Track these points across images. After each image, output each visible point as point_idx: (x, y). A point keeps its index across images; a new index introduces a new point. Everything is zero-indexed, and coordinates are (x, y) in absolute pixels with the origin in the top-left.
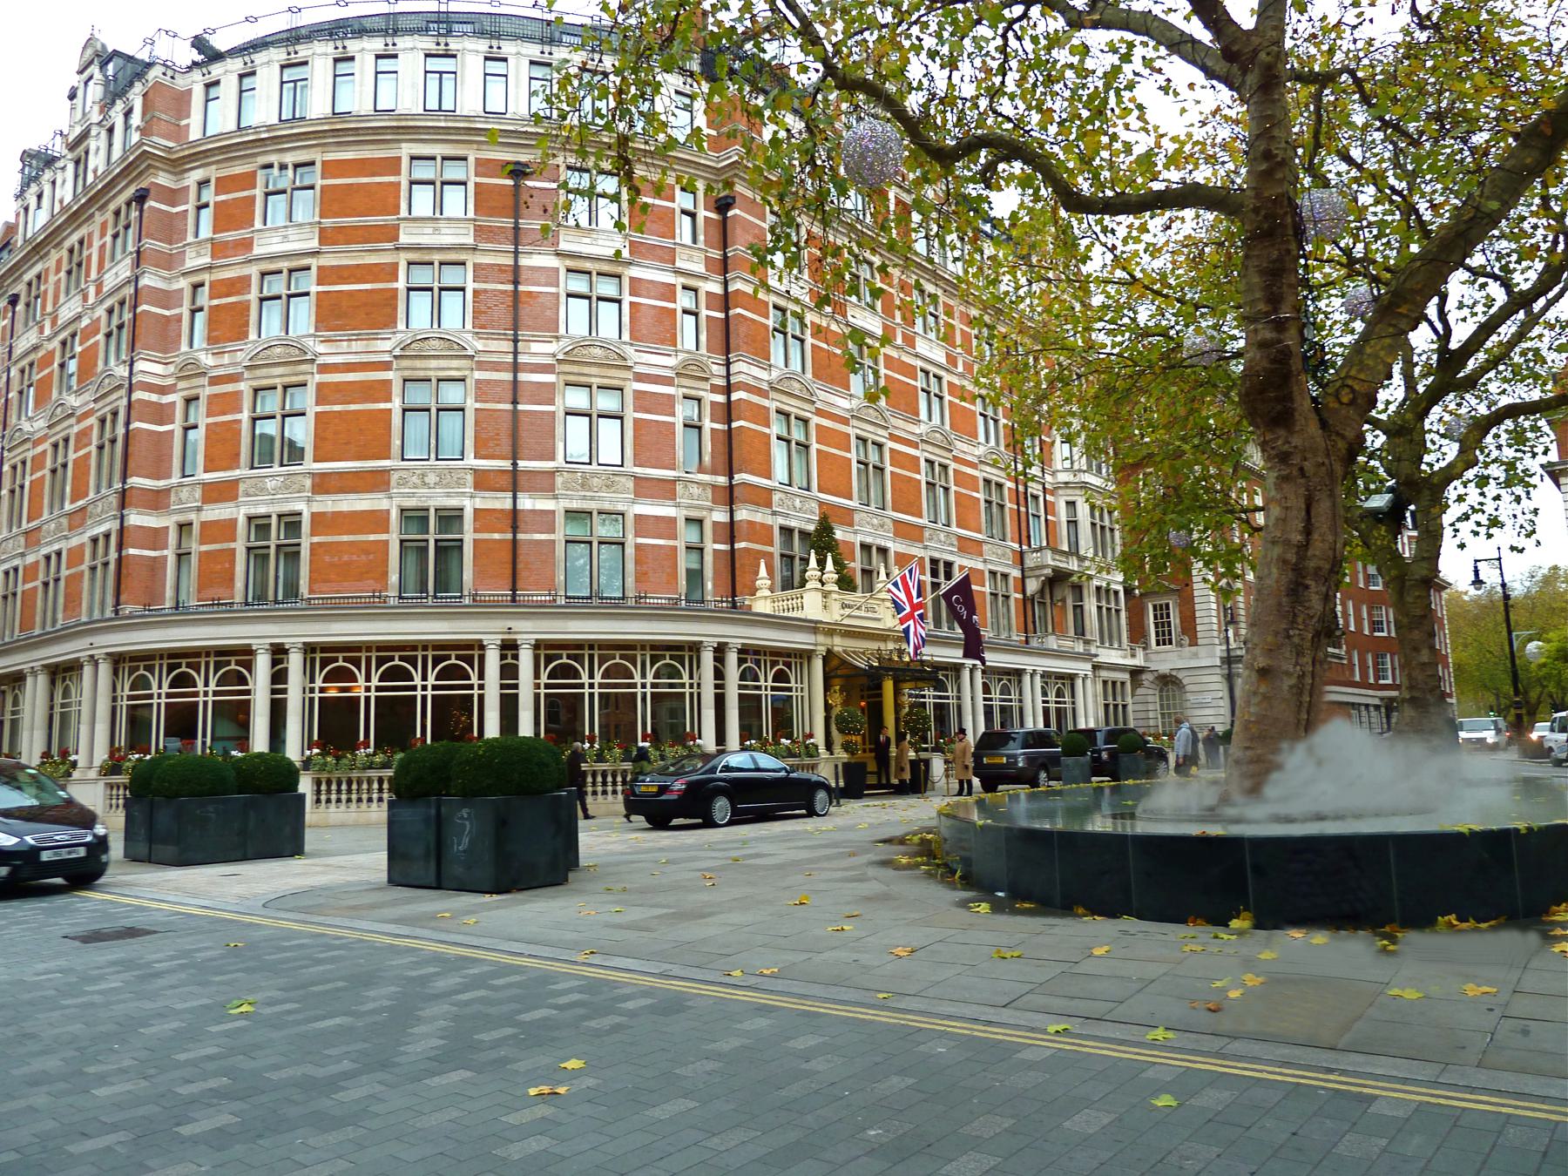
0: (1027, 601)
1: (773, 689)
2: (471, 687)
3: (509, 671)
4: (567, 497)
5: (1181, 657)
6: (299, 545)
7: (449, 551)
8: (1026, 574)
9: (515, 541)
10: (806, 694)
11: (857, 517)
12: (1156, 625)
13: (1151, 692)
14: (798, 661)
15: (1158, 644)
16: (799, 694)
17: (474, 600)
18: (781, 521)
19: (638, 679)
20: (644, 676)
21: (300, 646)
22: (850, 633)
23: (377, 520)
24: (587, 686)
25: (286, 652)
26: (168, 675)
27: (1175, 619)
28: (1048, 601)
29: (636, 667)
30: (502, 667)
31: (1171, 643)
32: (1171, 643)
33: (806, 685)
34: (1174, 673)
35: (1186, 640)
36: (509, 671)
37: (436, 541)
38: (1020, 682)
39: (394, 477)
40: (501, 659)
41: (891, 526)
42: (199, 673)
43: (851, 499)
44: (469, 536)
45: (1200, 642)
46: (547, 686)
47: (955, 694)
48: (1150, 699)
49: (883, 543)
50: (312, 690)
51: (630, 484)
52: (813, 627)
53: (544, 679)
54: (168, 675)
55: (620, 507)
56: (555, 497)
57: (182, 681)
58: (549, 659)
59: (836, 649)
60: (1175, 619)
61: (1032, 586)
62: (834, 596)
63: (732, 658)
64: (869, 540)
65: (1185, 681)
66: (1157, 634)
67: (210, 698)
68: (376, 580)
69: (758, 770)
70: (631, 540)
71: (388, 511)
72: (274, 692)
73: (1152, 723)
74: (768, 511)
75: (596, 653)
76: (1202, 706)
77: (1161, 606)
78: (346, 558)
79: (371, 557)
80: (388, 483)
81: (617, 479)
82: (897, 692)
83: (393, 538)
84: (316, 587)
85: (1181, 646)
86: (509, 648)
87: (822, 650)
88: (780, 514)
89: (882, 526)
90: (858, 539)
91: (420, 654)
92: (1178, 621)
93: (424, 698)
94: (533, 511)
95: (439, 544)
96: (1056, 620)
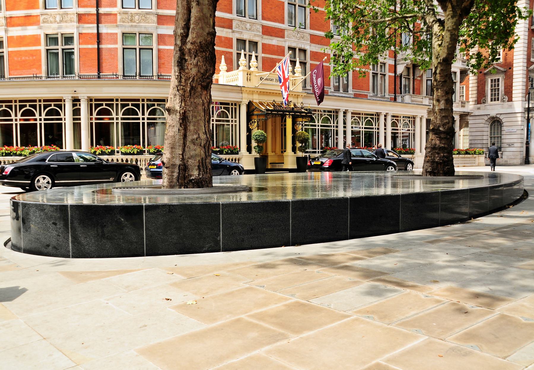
0: (397, 78)
1: (321, 126)
2: (139, 119)
3: (76, 112)
4: (122, 26)
5: (503, 108)
6: (3, 52)
7: (68, 55)
8: (397, 63)
9: (99, 49)
10: (238, 123)
11: (286, 33)
12: (492, 90)
13: (486, 126)
14: (234, 107)
15: (492, 100)
16: (234, 123)
17: (158, 78)
18: (238, 36)
19: (140, 116)
20: (143, 114)
21: (86, 98)
22: (263, 93)
23: (35, 40)
24: (141, 119)
25: (79, 100)
26: (44, 111)
27: (502, 87)
28: (411, 77)
29: (36, 110)
30: (74, 111)
31: (498, 100)
32: (498, 100)
33: (238, 119)
34: (498, 116)
35: (506, 98)
36: (76, 112)
37: (63, 49)
38: (378, 119)
39: (42, 18)
40: (73, 107)
41: (309, 37)
42: (36, 110)
43: (283, 22)
44: (76, 46)
45: (513, 99)
46: (45, 120)
47: (335, 124)
48: (486, 129)
49: (303, 47)
50: (91, 119)
51: (155, 19)
52: (240, 89)
53: (95, 115)
54: (44, 111)
55: (150, 31)
56: (117, 26)
57: (28, 113)
58: (97, 106)
59: (255, 101)
60: (502, 87)
61: (400, 69)
62: (254, 74)
63: (349, 115)
64: (293, 45)
65: (503, 121)
66: (492, 95)
67: (43, 122)
68: (37, 68)
69: (363, 156)
70: (155, 46)
71: (40, 35)
72: (74, 119)
73: (485, 142)
74: (230, 31)
75: (145, 103)
76: (511, 133)
77: (495, 80)
78: (23, 58)
79: (34, 58)
80: (39, 21)
81: (148, 16)
82: (294, 123)
83: (42, 48)
84: (12, 72)
85: (504, 101)
86: (76, 101)
87: (245, 102)
88: (238, 32)
89: (303, 38)
90: (286, 45)
91: (115, 103)
92: (503, 88)
93: (41, 124)
94: (107, 34)
95: (64, 51)
96: (416, 87)
